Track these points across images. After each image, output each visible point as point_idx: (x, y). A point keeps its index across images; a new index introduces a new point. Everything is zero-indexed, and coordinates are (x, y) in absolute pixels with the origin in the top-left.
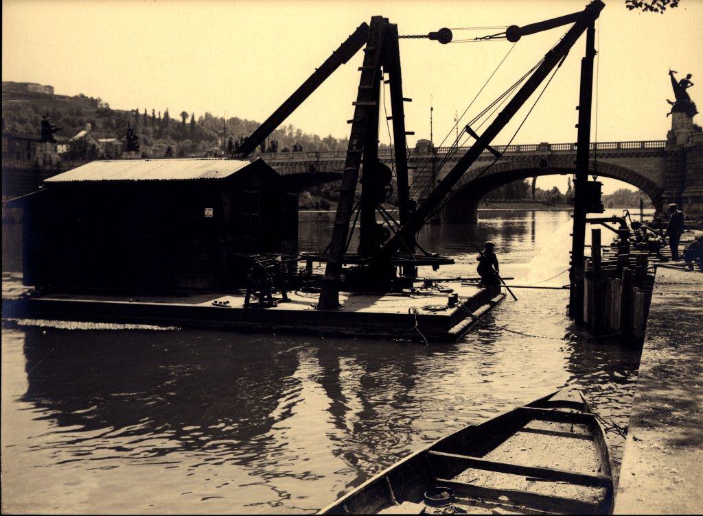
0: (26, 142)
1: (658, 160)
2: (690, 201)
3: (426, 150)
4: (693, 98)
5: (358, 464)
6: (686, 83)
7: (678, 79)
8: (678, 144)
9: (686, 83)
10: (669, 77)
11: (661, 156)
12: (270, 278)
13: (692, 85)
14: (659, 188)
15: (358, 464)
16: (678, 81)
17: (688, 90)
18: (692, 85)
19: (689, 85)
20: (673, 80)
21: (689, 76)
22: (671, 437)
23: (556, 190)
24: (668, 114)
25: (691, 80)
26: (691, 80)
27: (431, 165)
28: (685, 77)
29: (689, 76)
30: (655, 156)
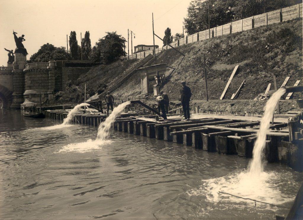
4: (25, 47)
5: (256, 212)
8: (20, 68)
10: (13, 36)
11: (10, 75)
12: (140, 114)
13: (25, 40)
14: (10, 91)
15: (256, 212)
17: (23, 43)
18: (25, 40)
20: (15, 37)
21: (23, 36)
22: (216, 141)
23: (150, 54)
26: (24, 38)
28: (21, 36)
30: (7, 75)
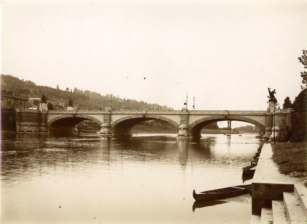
2: (182, 129)
3: (185, 111)
7: (271, 91)
16: (271, 92)
17: (274, 95)
21: (275, 90)
24: (268, 102)
25: (275, 91)
28: (273, 90)
29: (275, 90)
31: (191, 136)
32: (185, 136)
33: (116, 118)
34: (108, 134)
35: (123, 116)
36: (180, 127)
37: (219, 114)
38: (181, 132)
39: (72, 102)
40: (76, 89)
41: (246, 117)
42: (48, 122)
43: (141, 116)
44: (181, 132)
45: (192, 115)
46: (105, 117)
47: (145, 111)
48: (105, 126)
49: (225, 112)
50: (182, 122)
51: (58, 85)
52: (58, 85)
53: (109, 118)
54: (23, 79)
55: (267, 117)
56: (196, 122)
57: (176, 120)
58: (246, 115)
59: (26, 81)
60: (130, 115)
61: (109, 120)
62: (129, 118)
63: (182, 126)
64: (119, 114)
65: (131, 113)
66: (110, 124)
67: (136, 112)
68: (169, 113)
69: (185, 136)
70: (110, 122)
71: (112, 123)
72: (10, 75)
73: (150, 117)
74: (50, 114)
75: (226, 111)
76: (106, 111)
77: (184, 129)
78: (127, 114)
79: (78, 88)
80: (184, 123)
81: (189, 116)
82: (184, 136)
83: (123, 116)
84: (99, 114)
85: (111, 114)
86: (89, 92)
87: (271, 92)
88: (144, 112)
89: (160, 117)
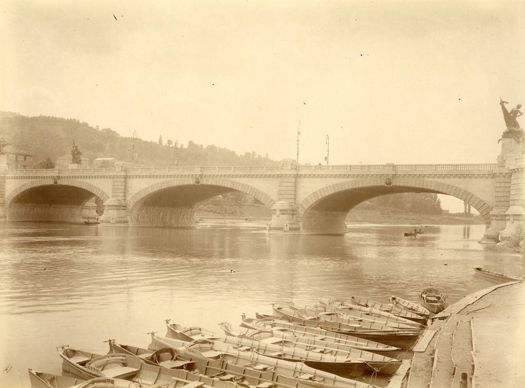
0: (23, 157)
1: (489, 182)
2: (278, 213)
3: (290, 168)
6: (515, 113)
7: (509, 108)
9: (515, 113)
10: (500, 107)
13: (522, 114)
16: (509, 111)
17: (518, 119)
18: (522, 114)
19: (519, 114)
21: (519, 107)
24: (499, 140)
25: (520, 110)
27: (293, 180)
28: (515, 107)
29: (519, 107)
31: (304, 228)
32: (285, 229)
33: (141, 187)
34: (117, 222)
35: (153, 182)
36: (273, 208)
37: (372, 173)
38: (275, 221)
39: (79, 153)
40: (191, 143)
41: (441, 180)
42: (6, 196)
43: (191, 182)
44: (275, 221)
45: (305, 176)
46: (116, 184)
47: (199, 169)
48: (111, 204)
49: (387, 168)
50: (281, 195)
51: (161, 136)
52: (161, 136)
53: (123, 187)
54: (97, 126)
55: (497, 179)
56: (315, 194)
57: (266, 188)
58: (440, 176)
59: (102, 130)
60: (168, 179)
61: (122, 194)
62: (164, 187)
63: (280, 204)
64: (318, 176)
65: (172, 173)
66: (125, 200)
67: (180, 172)
68: (269, 173)
69: (285, 229)
70: (125, 196)
71: (129, 198)
72: (75, 120)
73: (209, 184)
74: (305, 176)
75: (388, 165)
76: (117, 170)
77: (283, 212)
78: (160, 177)
79: (195, 142)
80: (286, 196)
81: (299, 179)
82: (281, 229)
83: (153, 182)
84: (265, 176)
85: (126, 177)
86: (215, 147)
87: (509, 111)
88: (197, 172)
89: (233, 183)
